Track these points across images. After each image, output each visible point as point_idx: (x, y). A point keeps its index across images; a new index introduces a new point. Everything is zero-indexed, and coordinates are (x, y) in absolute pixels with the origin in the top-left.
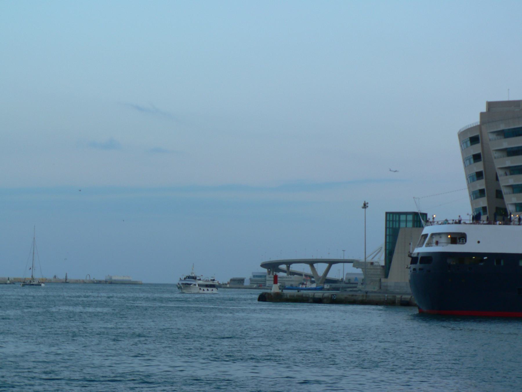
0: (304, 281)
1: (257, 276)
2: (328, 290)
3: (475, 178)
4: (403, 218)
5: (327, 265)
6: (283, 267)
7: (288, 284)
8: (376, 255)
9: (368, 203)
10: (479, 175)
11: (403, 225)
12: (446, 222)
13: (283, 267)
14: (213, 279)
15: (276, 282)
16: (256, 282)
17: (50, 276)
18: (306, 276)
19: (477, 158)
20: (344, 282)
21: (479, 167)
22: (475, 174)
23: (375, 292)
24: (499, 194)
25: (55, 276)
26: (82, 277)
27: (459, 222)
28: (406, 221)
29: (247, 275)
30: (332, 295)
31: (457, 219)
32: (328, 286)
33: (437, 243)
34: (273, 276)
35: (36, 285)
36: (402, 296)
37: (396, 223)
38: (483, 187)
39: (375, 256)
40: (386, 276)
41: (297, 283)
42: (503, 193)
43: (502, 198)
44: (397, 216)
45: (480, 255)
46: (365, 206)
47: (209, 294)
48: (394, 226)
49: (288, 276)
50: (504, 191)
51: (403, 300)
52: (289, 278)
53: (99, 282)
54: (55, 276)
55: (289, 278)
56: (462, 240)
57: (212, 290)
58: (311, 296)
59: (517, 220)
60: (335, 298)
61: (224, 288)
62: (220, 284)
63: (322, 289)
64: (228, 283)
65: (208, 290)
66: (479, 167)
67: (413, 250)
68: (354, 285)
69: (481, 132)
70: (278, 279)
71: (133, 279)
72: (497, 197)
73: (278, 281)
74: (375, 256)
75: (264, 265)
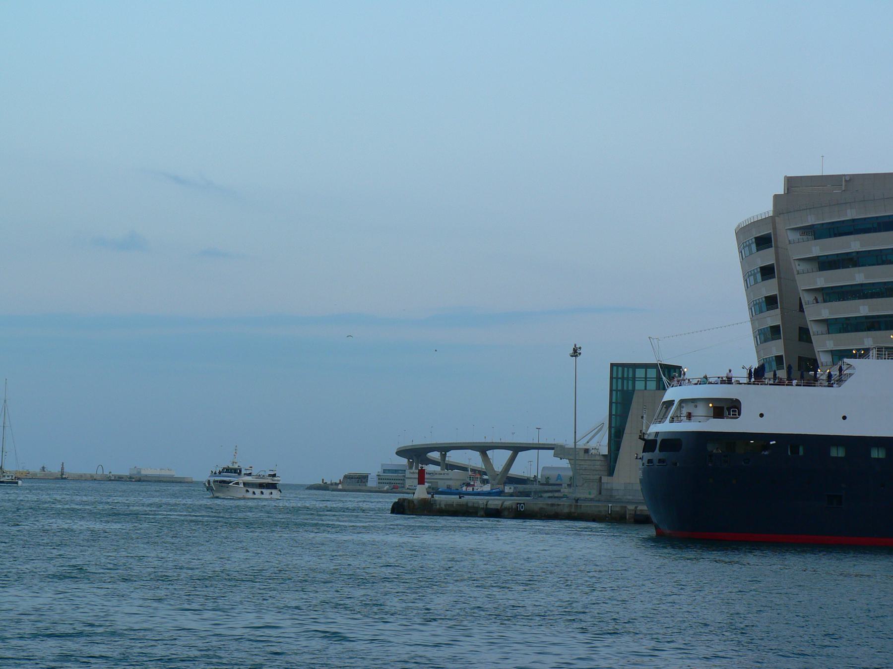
0: (470, 480)
1: (389, 471)
2: (511, 495)
3: (764, 306)
4: (640, 373)
5: (509, 453)
6: (435, 455)
7: (442, 486)
8: (593, 437)
9: (580, 348)
10: (771, 302)
11: (640, 385)
12: (705, 381)
13: (435, 455)
14: (272, 473)
15: (421, 481)
16: (388, 481)
17: (34, 468)
18: (473, 470)
19: (767, 272)
20: (539, 482)
21: (770, 288)
22: (764, 299)
23: (592, 500)
24: (804, 335)
25: (43, 468)
26: (89, 470)
27: (729, 381)
28: (646, 379)
29: (373, 469)
30: (518, 504)
31: (724, 374)
32: (510, 488)
33: (689, 416)
34: (417, 471)
35: (7, 483)
36: (636, 507)
37: (628, 383)
38: (778, 322)
39: (591, 439)
40: (611, 472)
41: (458, 483)
42: (811, 334)
43: (810, 341)
44: (631, 371)
45: (763, 438)
46: (576, 353)
47: (267, 499)
48: (625, 388)
49: (442, 472)
50: (813, 328)
51: (638, 513)
52: (444, 474)
53: (120, 479)
54: (43, 468)
55: (444, 474)
56: (733, 411)
57: (271, 493)
58: (482, 506)
59: (824, 377)
60: (522, 510)
61: (333, 490)
62: (326, 483)
63: (500, 493)
64: (340, 483)
65: (262, 493)
66: (770, 288)
67: (648, 428)
68: (555, 488)
69: (774, 228)
70: (426, 476)
71: (177, 474)
72: (801, 339)
73: (426, 480)
74: (591, 439)
75: (401, 453)
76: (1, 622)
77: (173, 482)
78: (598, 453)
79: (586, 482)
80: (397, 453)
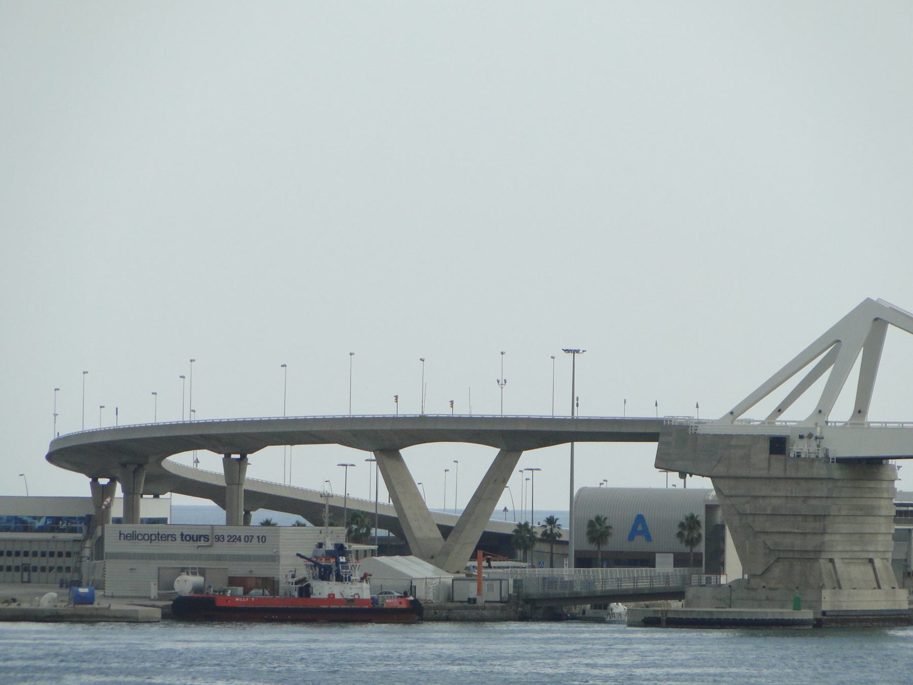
76: (901, 600)
77: (884, 620)
78: (821, 455)
79: (778, 560)
80: (51, 457)
